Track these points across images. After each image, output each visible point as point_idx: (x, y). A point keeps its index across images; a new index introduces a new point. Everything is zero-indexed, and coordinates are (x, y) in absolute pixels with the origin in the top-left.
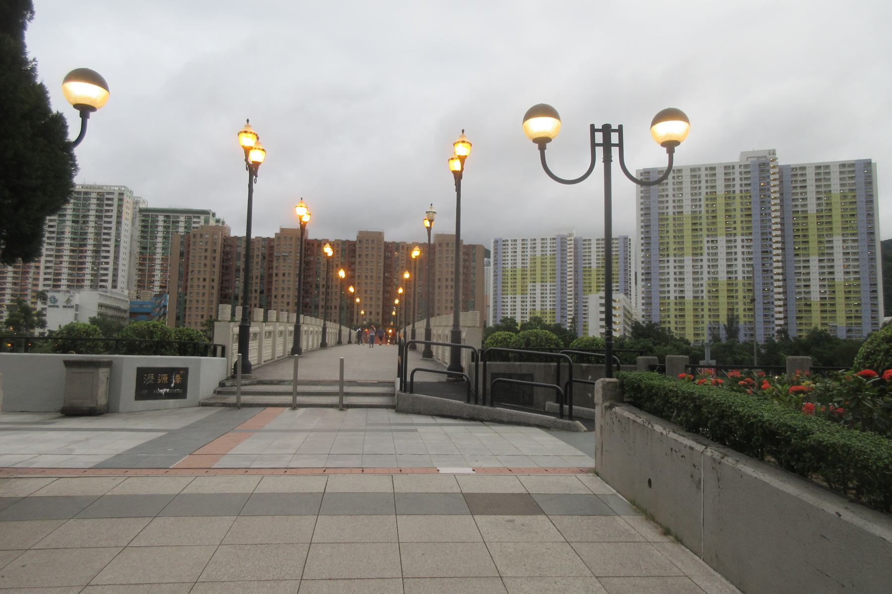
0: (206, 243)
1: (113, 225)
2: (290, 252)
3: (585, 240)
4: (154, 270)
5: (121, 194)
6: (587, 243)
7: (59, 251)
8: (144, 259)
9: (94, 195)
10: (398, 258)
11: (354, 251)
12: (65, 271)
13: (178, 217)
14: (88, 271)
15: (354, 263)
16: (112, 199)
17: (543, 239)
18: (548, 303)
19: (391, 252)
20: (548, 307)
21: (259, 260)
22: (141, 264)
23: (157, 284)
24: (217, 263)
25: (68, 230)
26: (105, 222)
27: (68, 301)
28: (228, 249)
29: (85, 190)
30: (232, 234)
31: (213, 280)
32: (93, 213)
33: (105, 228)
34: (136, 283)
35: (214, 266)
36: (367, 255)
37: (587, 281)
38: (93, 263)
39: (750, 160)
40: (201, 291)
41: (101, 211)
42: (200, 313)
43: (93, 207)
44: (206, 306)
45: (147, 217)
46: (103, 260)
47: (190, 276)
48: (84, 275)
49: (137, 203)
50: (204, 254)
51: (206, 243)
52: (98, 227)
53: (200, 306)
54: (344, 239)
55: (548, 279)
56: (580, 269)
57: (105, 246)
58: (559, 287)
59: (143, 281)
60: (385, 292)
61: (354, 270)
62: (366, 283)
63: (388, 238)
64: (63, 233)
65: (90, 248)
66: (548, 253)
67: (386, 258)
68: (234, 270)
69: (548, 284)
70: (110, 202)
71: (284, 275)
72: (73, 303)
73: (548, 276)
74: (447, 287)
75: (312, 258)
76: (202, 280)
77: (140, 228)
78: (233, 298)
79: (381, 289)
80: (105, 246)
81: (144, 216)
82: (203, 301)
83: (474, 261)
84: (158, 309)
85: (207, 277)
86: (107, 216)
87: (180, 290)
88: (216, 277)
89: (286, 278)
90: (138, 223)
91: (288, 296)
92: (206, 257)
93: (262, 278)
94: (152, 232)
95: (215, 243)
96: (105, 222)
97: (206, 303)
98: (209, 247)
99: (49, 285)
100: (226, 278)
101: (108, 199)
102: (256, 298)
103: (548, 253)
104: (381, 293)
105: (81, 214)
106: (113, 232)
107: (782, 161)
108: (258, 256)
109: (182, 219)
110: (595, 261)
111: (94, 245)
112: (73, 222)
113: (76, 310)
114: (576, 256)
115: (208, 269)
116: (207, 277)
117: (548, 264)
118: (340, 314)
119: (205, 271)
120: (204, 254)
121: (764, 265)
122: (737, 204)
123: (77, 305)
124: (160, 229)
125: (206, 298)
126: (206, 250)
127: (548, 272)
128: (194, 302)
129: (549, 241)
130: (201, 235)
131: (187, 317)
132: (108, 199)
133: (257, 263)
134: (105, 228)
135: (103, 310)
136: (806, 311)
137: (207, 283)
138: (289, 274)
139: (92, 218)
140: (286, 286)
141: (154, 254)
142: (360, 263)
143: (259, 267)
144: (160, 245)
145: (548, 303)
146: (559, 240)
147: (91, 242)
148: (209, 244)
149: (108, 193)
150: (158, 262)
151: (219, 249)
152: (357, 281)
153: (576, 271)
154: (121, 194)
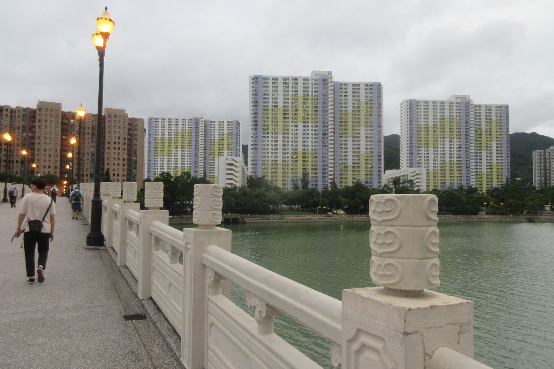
3: (211, 122)
19: (68, 119)
36: (46, 121)
37: (212, 149)
39: (317, 76)
54: (25, 106)
56: (208, 141)
62: (45, 143)
67: (63, 124)
69: (186, 150)
74: (115, 148)
83: (137, 130)
107: (335, 79)
121: (323, 142)
122: (310, 103)
127: (187, 142)
136: (345, 170)
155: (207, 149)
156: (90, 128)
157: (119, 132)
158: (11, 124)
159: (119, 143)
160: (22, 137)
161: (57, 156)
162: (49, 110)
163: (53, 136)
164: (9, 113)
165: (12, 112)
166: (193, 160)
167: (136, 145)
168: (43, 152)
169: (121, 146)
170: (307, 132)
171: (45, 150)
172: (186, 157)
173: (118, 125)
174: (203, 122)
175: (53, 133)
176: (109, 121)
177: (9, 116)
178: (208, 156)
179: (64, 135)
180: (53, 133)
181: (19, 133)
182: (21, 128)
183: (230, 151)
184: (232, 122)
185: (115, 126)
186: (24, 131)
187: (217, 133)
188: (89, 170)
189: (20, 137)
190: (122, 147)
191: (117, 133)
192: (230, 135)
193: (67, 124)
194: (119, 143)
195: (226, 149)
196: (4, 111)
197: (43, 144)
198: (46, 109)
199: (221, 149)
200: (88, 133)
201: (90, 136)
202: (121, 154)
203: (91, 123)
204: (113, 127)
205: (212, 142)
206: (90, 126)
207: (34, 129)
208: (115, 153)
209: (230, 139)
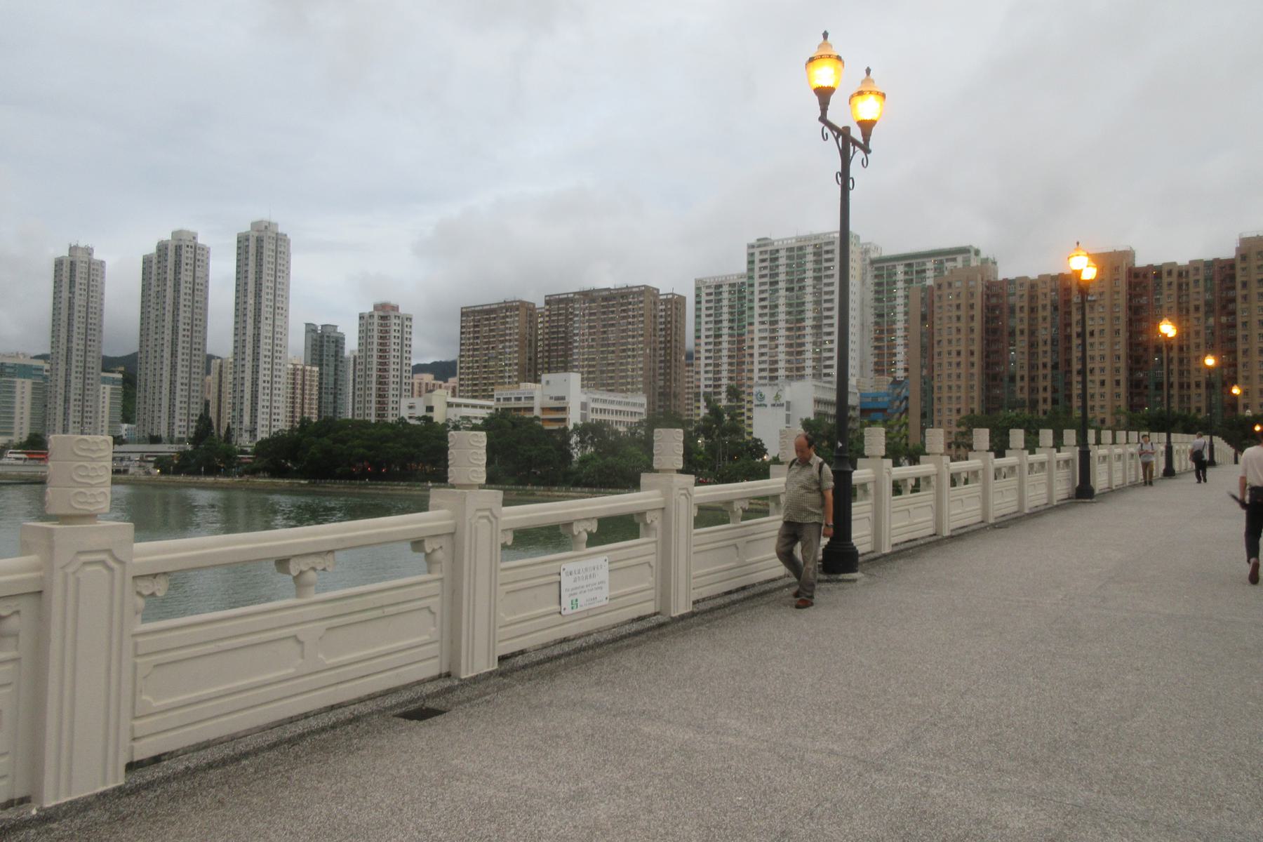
4: (894, 346)
7: (774, 331)
8: (882, 332)
9: (810, 250)
11: (1232, 277)
12: (782, 357)
13: (924, 264)
14: (809, 355)
15: (1233, 300)
21: (1048, 313)
22: (877, 339)
23: (901, 365)
24: (977, 325)
25: (782, 301)
27: (777, 397)
28: (994, 301)
29: (799, 244)
30: (1000, 277)
32: (810, 274)
33: (826, 293)
34: (872, 366)
35: (972, 330)
38: (814, 343)
40: (954, 370)
41: (820, 270)
42: (954, 407)
43: (810, 266)
44: (963, 394)
45: (882, 269)
46: (825, 338)
47: (936, 350)
48: (804, 360)
49: (866, 251)
50: (954, 313)
51: (958, 295)
52: (817, 293)
53: (954, 395)
54: (1208, 256)
59: (882, 365)
61: (1233, 313)
64: (776, 306)
65: (809, 322)
68: (1006, 333)
70: (830, 256)
72: (783, 401)
75: (1144, 300)
76: (954, 354)
77: (872, 288)
78: (1006, 379)
81: (877, 269)
82: (959, 387)
84: (897, 403)
85: (962, 348)
87: (925, 372)
88: (977, 347)
90: (870, 281)
91: (1102, 370)
92: (958, 318)
93: (1054, 342)
94: (890, 291)
95: (972, 295)
97: (963, 390)
99: (765, 378)
100: (994, 347)
101: (827, 252)
102: (1045, 377)
105: (795, 278)
108: (1044, 307)
109: (930, 265)
111: (814, 318)
112: (787, 290)
113: (788, 409)
116: (962, 348)
118: (1209, 397)
119: (959, 340)
120: (954, 313)
123: (788, 403)
124: (900, 285)
125: (962, 382)
126: (958, 307)
128: (945, 389)
130: (950, 285)
131: (935, 413)
132: (827, 252)
133: (1044, 319)
134: (826, 293)
135: (822, 408)
137: (962, 359)
138: (1102, 331)
139: (809, 282)
141: (894, 322)
142: (1245, 297)
144: (900, 309)
147: (809, 314)
149: (828, 244)
150: (900, 333)
151: (978, 302)
152: (1241, 373)
158: (1179, 303)
160: (1207, 328)
164: (1174, 279)
165: (1180, 274)
177: (1175, 286)
181: (1198, 319)
182: (1202, 309)
189: (1202, 328)
196: (1165, 275)
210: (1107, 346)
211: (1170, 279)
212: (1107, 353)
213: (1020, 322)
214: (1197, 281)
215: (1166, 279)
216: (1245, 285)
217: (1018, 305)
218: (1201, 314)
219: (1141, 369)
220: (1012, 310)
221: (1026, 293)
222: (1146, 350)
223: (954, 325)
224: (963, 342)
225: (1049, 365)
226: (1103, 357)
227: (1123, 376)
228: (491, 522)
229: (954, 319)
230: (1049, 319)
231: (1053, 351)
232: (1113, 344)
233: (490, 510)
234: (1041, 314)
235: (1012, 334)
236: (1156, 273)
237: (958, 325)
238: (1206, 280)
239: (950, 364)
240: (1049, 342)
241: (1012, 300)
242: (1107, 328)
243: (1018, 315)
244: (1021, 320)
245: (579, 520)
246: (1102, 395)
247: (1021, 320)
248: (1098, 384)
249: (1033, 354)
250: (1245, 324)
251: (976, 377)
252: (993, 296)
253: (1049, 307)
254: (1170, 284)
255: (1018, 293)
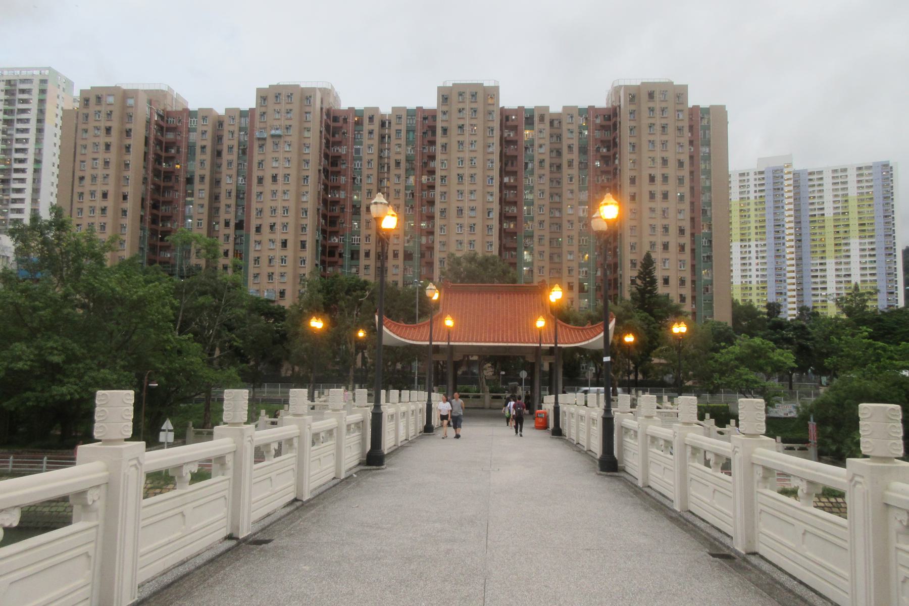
0: (109, 114)
1: (32, 136)
2: (288, 128)
3: (810, 174)
5: (44, 82)
6: (815, 177)
10: (532, 143)
16: (28, 91)
17: (742, 175)
18: (754, 273)
19: (515, 128)
20: (754, 280)
21: (234, 157)
26: (18, 130)
28: (170, 136)
31: (125, 197)
36: (461, 127)
37: (817, 237)
50: (103, 139)
51: (109, 114)
54: (412, 105)
55: (753, 236)
56: (805, 219)
57: (17, 171)
58: (773, 247)
60: (504, 217)
62: (461, 193)
63: (508, 100)
66: (752, 195)
67: (505, 142)
68: (182, 180)
69: (753, 243)
70: (25, 96)
71: (274, 178)
73: (753, 231)
74: (652, 196)
75: (343, 150)
76: (99, 195)
79: (496, 207)
80: (17, 171)
83: (708, 144)
85: (111, 188)
86: (20, 121)
88: (134, 189)
89: (280, 187)
92: (108, 146)
96: (18, 130)
98: (115, 124)
101: (23, 91)
103: (752, 195)
104: (495, 215)
106: (31, 147)
108: (230, 148)
110: (831, 205)
114: (797, 199)
115: (112, 171)
116: (111, 188)
117: (752, 213)
120: (103, 139)
127: (753, 225)
129: (752, 177)
132: (23, 91)
133: (230, 163)
137: (110, 203)
138: (286, 176)
140: (279, 204)
143: (233, 172)
145: (754, 273)
146: (771, 175)
148: (115, 116)
149: (24, 81)
151: (139, 131)
153: (798, 222)
154: (44, 82)
155: (804, 238)
156: (576, 149)
157: (664, 143)
158: (380, 157)
159: (665, 178)
160: (407, 188)
161: (490, 228)
162: (468, 96)
163: (479, 172)
164: (376, 126)
165: (383, 124)
166: (771, 266)
167: (709, 189)
168: (454, 220)
169: (671, 187)
170: (748, 273)
171: (460, 211)
172: (754, 261)
173: (659, 122)
174: (791, 176)
175: (479, 162)
176: (632, 113)
177: (376, 136)
178: (806, 256)
179: (508, 174)
180: (479, 162)
181: (399, 177)
182: (403, 165)
183: (867, 240)
184: (869, 168)
185: (651, 126)
186: (409, 171)
187: (828, 197)
188: (574, 273)
189: (401, 187)
190: (675, 192)
191: (658, 145)
192: (864, 200)
193: (514, 142)
194: (665, 178)
195: (857, 234)
196: (366, 121)
197: (454, 196)
198: (460, 94)
199: (842, 235)
200: (570, 164)
201: (575, 172)
202: (672, 213)
203: (575, 135)
204: (645, 131)
205: (817, 220)
206: (575, 143)
207: (432, 164)
208: (652, 210)
209: (865, 209)
210: (291, 196)
211: (371, 127)
212: (292, 205)
213: (200, 166)
214: (398, 132)
215: (367, 126)
216: (445, 131)
217: (199, 144)
218: (402, 171)
219: (335, 233)
220: (191, 148)
221: (209, 130)
222: (342, 209)
223: (102, 155)
224: (112, 180)
225: (232, 224)
226: (286, 210)
227: (310, 237)
228: (137, 468)
229: (102, 147)
230: (235, 164)
231: (237, 205)
232: (299, 195)
233: (137, 458)
234: (226, 157)
235: (190, 181)
236: (358, 118)
237: (107, 156)
238: (408, 131)
239: (93, 210)
240: (234, 194)
241: (193, 137)
242: (293, 172)
243: (199, 156)
244: (202, 163)
245: (187, 463)
246: (283, 260)
247: (202, 163)
248: (279, 244)
249: (213, 211)
250: (443, 178)
251: (128, 230)
252: (169, 129)
253: (235, 149)
254: (371, 132)
255: (200, 129)
